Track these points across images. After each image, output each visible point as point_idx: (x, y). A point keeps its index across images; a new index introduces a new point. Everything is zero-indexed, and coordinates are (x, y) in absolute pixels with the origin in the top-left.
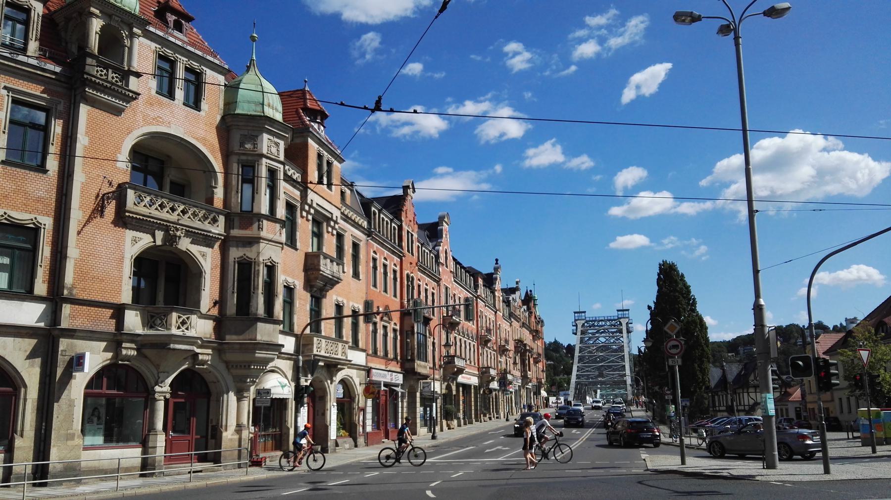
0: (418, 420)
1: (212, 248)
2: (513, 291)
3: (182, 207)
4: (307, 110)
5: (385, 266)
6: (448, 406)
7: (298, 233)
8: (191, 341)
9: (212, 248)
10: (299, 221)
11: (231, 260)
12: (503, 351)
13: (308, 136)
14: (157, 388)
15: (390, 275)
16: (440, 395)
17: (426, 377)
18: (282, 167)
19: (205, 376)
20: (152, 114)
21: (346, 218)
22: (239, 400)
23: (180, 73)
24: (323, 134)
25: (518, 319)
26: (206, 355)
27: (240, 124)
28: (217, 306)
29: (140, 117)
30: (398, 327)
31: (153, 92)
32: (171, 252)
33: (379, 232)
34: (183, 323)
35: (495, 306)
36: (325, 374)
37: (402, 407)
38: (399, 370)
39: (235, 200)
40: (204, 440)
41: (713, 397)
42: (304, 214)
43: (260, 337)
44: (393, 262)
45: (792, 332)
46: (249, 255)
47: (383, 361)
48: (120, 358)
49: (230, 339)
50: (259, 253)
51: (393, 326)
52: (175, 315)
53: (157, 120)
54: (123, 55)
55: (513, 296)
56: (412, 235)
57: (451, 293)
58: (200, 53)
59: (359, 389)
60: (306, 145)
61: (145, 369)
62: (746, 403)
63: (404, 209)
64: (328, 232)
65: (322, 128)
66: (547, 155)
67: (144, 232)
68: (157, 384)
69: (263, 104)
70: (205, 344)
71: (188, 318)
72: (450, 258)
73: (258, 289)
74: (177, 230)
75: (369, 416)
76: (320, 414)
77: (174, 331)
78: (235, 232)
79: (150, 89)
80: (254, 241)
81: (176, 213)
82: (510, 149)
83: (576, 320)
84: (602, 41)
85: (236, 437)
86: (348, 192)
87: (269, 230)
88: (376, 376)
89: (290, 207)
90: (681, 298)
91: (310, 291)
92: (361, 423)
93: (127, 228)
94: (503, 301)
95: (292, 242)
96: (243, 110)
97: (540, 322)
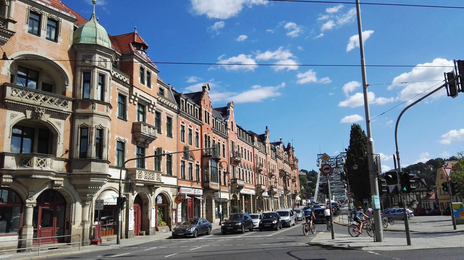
0: (214, 215)
1: (65, 119)
2: (278, 143)
3: (43, 97)
4: (135, 44)
5: (190, 130)
6: (235, 207)
7: (127, 112)
8: (48, 173)
9: (65, 119)
10: (128, 105)
11: (76, 126)
12: (271, 176)
13: (133, 57)
14: (28, 201)
15: (194, 135)
16: (229, 200)
17: (217, 191)
18: (108, 73)
19: (62, 193)
20: (25, 44)
21: (162, 104)
22: (83, 206)
23: (45, 22)
24: (145, 57)
25: (281, 159)
26: (60, 181)
27: (82, 49)
28: (68, 153)
29: (17, 46)
30: (200, 164)
31: (26, 32)
32: (38, 122)
33: (186, 111)
34: (42, 163)
35: (266, 152)
36: (147, 191)
37: (203, 208)
38: (201, 187)
39: (80, 92)
40: (62, 230)
41: (391, 198)
42: (132, 101)
43: (92, 170)
44: (195, 128)
45: (438, 162)
46: (87, 123)
47: (190, 182)
48: (2, 184)
49: (75, 171)
50: (92, 122)
51: (196, 163)
52: (35, 159)
53: (28, 48)
54: (5, 10)
55: (278, 146)
56: (208, 113)
57: (236, 145)
58: (57, 10)
59: (173, 199)
60: (132, 62)
61: (21, 190)
62: (408, 201)
63: (203, 99)
64: (149, 111)
65: (144, 53)
66: (309, 77)
67: (19, 111)
68: (27, 198)
69: (96, 38)
70: (58, 175)
71: (44, 160)
72: (235, 126)
73: (92, 142)
74: (40, 110)
75: (179, 213)
76: (145, 213)
77: (35, 167)
78: (79, 111)
79: (24, 30)
80: (89, 116)
81: (39, 100)
82: (289, 75)
83: (318, 159)
84: (335, 21)
85: (81, 228)
86: (166, 90)
87: (98, 109)
88: (184, 191)
89: (122, 97)
90: (363, 144)
91: (137, 144)
92: (174, 217)
93: (7, 109)
94: (271, 149)
95: (123, 116)
96: (84, 41)
97: (295, 160)
